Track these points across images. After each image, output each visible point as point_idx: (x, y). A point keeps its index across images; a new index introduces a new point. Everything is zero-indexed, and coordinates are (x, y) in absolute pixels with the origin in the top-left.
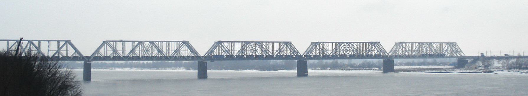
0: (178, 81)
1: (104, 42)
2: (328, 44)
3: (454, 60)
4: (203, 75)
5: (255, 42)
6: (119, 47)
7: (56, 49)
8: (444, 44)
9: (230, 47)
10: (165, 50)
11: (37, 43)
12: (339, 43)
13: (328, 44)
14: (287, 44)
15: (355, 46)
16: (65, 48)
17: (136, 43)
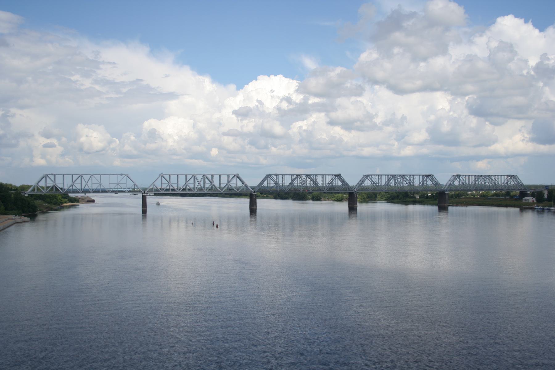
0: (331, 219)
1: (267, 175)
2: (415, 177)
3: (407, 24)
4: (352, 209)
5: (400, 175)
6: (174, 180)
7: (70, 183)
8: (473, 177)
9: (319, 181)
10: (320, 183)
11: (210, 177)
12: (478, 176)
13: (418, 176)
14: (338, 176)
15: (493, 178)
16: (233, 181)
17: (295, 176)
